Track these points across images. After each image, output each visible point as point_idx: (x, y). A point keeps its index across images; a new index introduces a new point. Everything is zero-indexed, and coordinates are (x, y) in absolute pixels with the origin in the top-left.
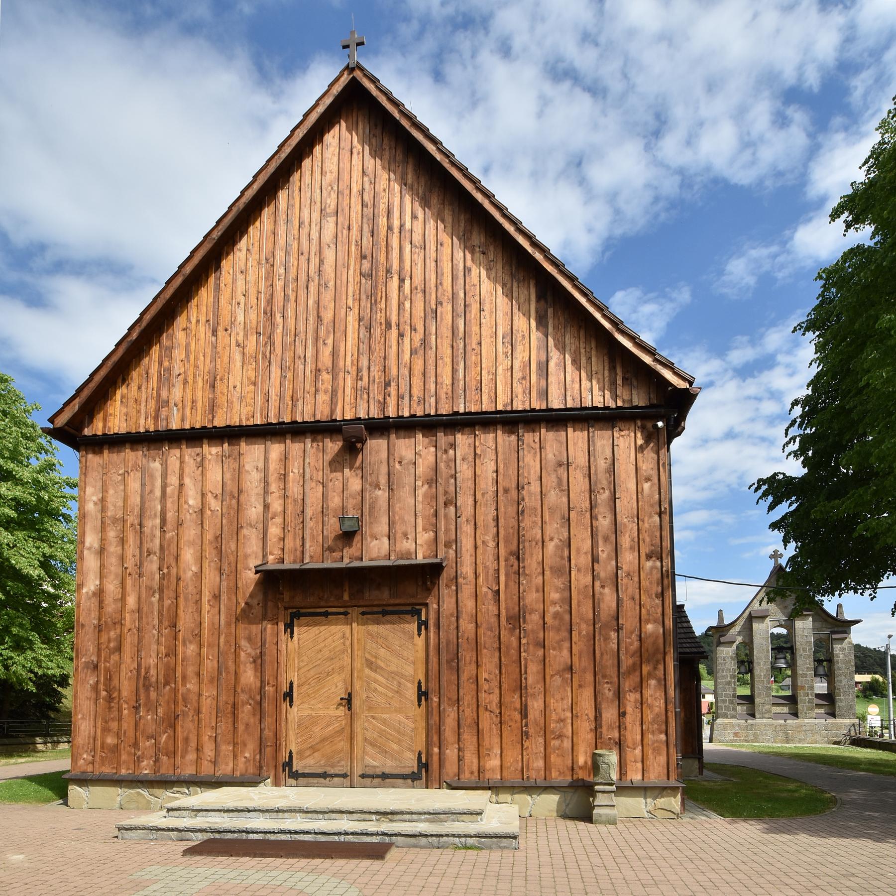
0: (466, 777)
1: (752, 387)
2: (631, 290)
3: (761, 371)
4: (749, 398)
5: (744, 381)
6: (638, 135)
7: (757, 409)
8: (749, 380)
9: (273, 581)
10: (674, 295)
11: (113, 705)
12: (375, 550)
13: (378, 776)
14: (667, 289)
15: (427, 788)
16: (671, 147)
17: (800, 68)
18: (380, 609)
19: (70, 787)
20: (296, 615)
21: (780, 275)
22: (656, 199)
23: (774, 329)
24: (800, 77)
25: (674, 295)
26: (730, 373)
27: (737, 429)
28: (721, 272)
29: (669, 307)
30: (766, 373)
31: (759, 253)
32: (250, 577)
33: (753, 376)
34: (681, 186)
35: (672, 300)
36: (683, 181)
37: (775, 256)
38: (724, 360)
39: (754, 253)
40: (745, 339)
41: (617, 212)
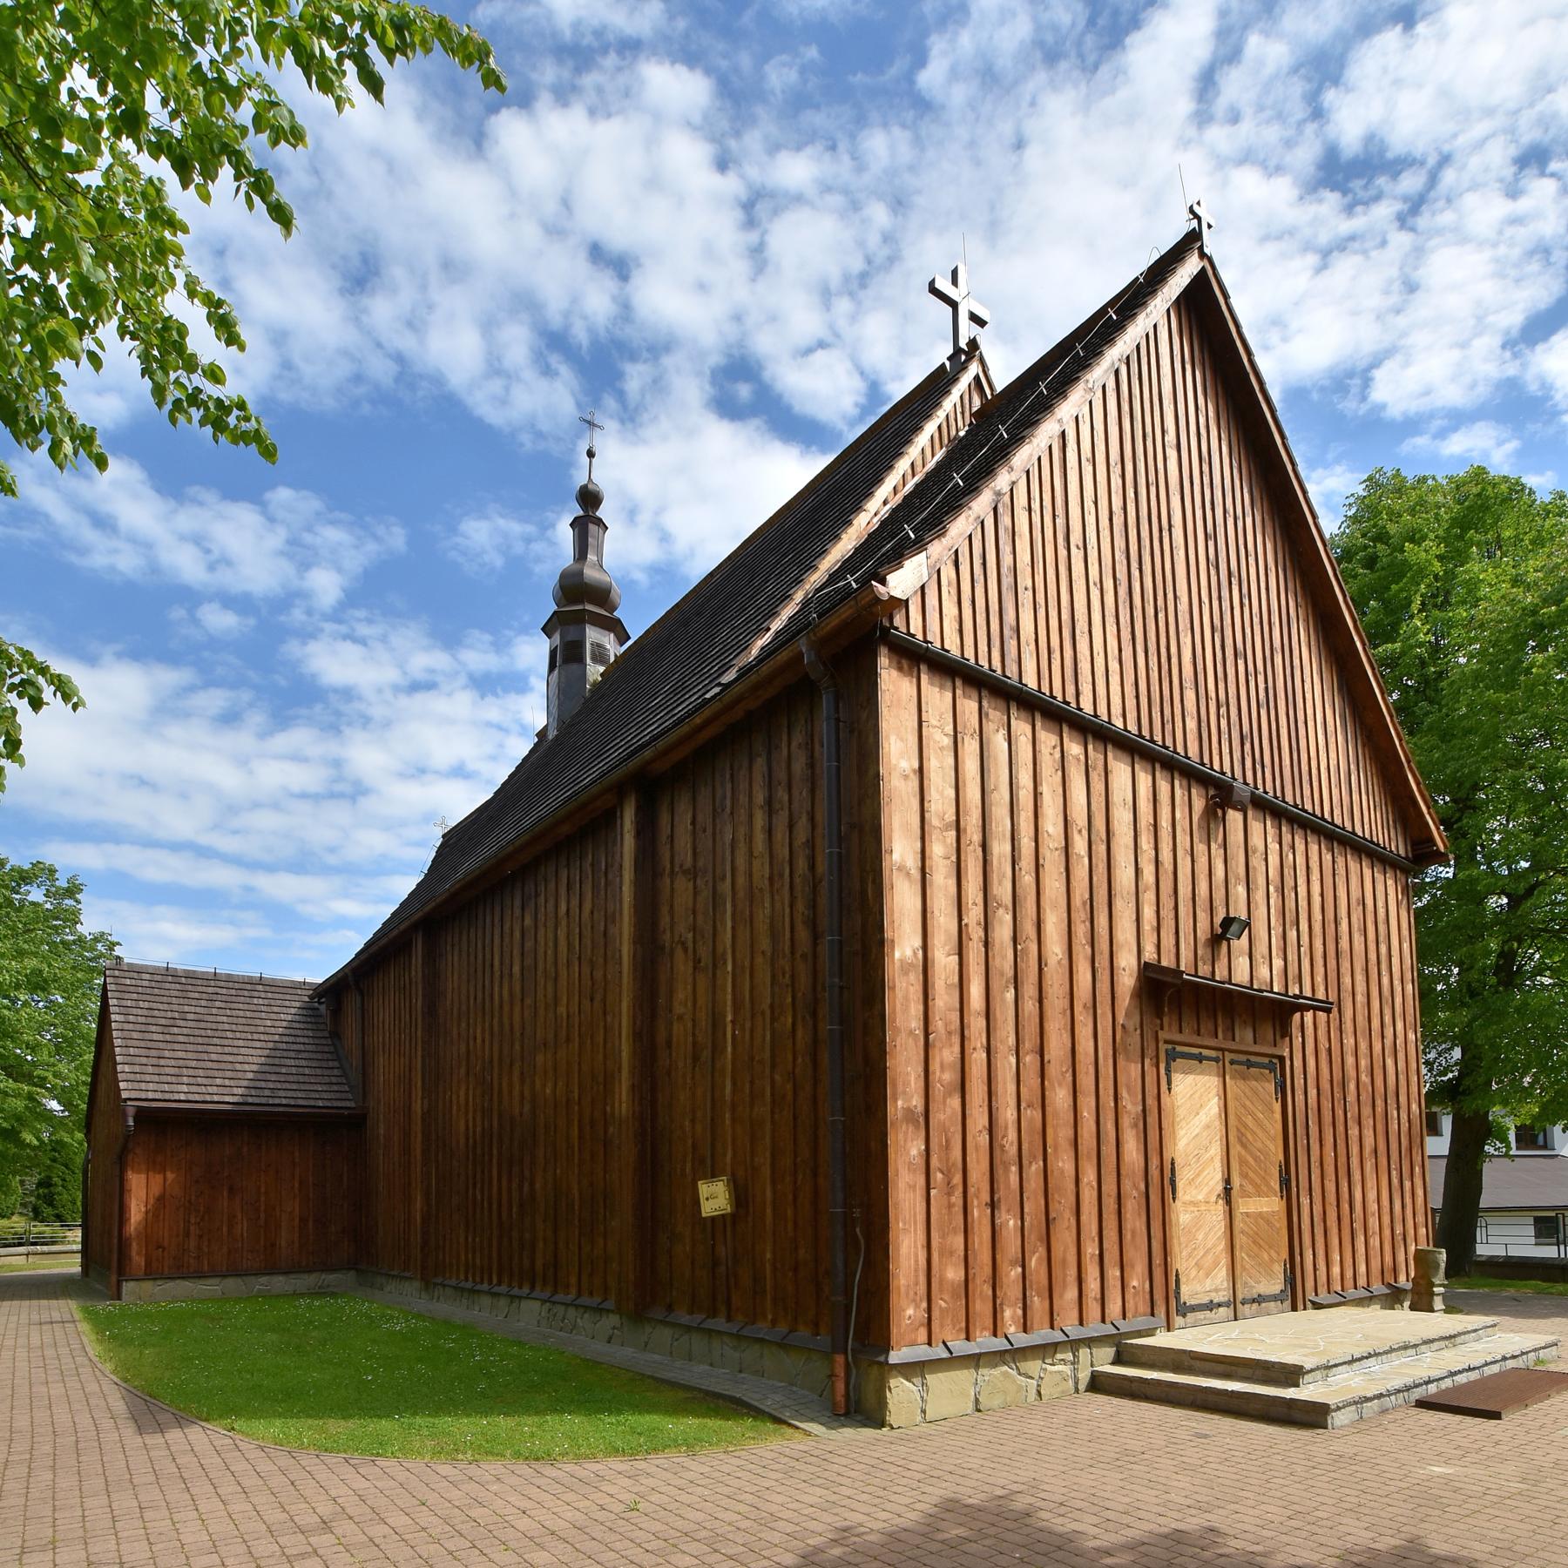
0: (1351, 1293)
1: (492, 711)
2: (304, 493)
3: (506, 690)
4: (489, 724)
5: (482, 697)
6: (334, 267)
7: (501, 746)
8: (490, 699)
9: (1160, 990)
10: (381, 530)
11: (953, 1199)
12: (1241, 968)
13: (1254, 1301)
14: (367, 519)
15: (1294, 1308)
16: (383, 310)
17: (567, 314)
18: (1243, 1058)
19: (893, 1383)
20: (1172, 1057)
21: (538, 569)
22: (358, 378)
23: (526, 638)
24: (567, 327)
25: (381, 530)
26: (462, 680)
27: (471, 766)
28: (453, 529)
29: (371, 547)
30: (513, 696)
31: (516, 528)
32: (1127, 980)
33: (496, 695)
34: (398, 379)
35: (377, 539)
36: (401, 373)
37: (528, 540)
38: (453, 656)
39: (501, 522)
40: (487, 637)
41: (287, 365)
